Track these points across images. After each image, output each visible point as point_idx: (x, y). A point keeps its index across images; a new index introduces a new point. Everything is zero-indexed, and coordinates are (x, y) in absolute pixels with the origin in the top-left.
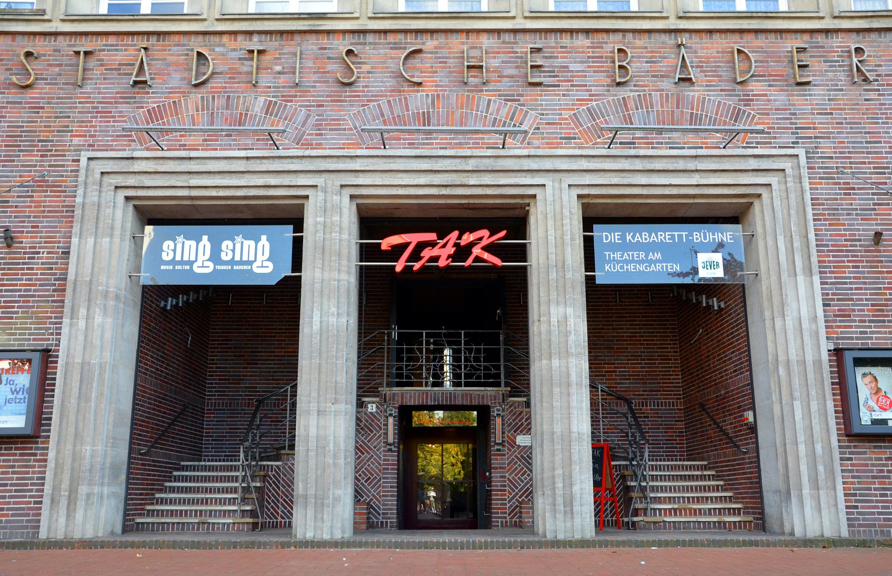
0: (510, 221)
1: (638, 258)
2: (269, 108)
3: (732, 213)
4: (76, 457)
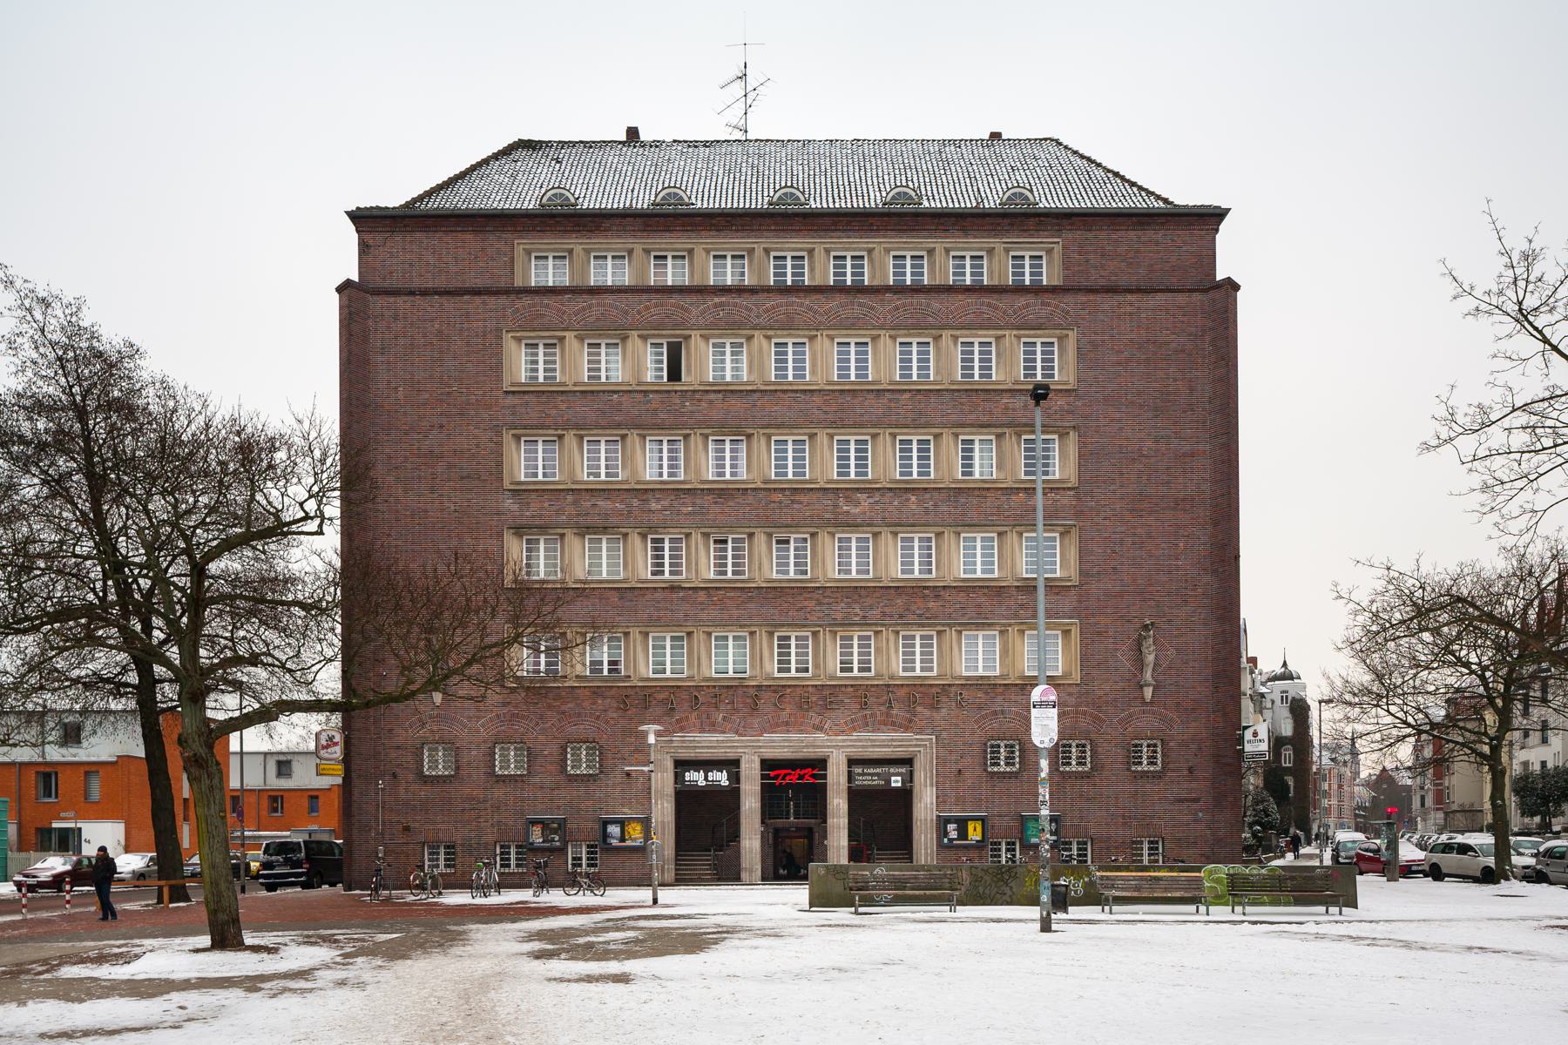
0: (822, 763)
1: (868, 779)
3: (908, 762)
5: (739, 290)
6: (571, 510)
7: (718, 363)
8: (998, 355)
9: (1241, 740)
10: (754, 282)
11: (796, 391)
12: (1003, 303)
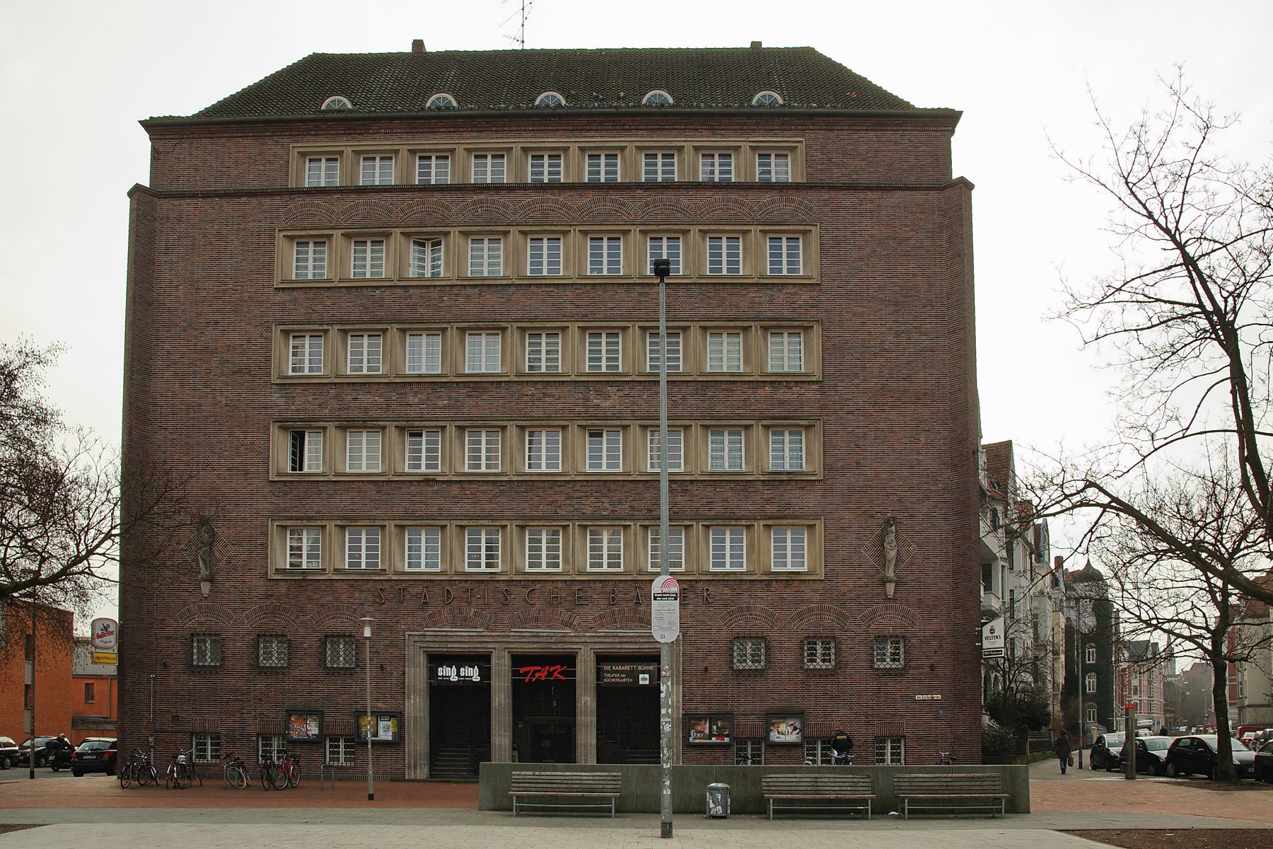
0: (569, 660)
1: (616, 675)
2: (476, 614)
4: (415, 751)
5: (497, 188)
6: (333, 404)
7: (693, 258)
8: (744, 249)
9: (979, 637)
10: (512, 181)
11: (550, 285)
12: (751, 198)
